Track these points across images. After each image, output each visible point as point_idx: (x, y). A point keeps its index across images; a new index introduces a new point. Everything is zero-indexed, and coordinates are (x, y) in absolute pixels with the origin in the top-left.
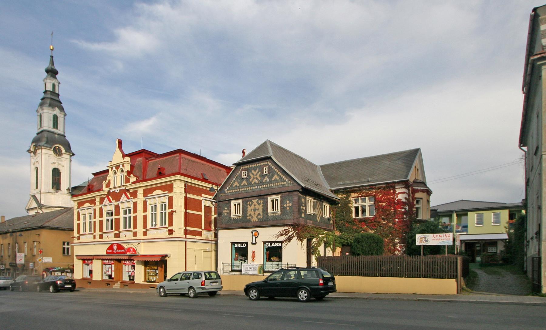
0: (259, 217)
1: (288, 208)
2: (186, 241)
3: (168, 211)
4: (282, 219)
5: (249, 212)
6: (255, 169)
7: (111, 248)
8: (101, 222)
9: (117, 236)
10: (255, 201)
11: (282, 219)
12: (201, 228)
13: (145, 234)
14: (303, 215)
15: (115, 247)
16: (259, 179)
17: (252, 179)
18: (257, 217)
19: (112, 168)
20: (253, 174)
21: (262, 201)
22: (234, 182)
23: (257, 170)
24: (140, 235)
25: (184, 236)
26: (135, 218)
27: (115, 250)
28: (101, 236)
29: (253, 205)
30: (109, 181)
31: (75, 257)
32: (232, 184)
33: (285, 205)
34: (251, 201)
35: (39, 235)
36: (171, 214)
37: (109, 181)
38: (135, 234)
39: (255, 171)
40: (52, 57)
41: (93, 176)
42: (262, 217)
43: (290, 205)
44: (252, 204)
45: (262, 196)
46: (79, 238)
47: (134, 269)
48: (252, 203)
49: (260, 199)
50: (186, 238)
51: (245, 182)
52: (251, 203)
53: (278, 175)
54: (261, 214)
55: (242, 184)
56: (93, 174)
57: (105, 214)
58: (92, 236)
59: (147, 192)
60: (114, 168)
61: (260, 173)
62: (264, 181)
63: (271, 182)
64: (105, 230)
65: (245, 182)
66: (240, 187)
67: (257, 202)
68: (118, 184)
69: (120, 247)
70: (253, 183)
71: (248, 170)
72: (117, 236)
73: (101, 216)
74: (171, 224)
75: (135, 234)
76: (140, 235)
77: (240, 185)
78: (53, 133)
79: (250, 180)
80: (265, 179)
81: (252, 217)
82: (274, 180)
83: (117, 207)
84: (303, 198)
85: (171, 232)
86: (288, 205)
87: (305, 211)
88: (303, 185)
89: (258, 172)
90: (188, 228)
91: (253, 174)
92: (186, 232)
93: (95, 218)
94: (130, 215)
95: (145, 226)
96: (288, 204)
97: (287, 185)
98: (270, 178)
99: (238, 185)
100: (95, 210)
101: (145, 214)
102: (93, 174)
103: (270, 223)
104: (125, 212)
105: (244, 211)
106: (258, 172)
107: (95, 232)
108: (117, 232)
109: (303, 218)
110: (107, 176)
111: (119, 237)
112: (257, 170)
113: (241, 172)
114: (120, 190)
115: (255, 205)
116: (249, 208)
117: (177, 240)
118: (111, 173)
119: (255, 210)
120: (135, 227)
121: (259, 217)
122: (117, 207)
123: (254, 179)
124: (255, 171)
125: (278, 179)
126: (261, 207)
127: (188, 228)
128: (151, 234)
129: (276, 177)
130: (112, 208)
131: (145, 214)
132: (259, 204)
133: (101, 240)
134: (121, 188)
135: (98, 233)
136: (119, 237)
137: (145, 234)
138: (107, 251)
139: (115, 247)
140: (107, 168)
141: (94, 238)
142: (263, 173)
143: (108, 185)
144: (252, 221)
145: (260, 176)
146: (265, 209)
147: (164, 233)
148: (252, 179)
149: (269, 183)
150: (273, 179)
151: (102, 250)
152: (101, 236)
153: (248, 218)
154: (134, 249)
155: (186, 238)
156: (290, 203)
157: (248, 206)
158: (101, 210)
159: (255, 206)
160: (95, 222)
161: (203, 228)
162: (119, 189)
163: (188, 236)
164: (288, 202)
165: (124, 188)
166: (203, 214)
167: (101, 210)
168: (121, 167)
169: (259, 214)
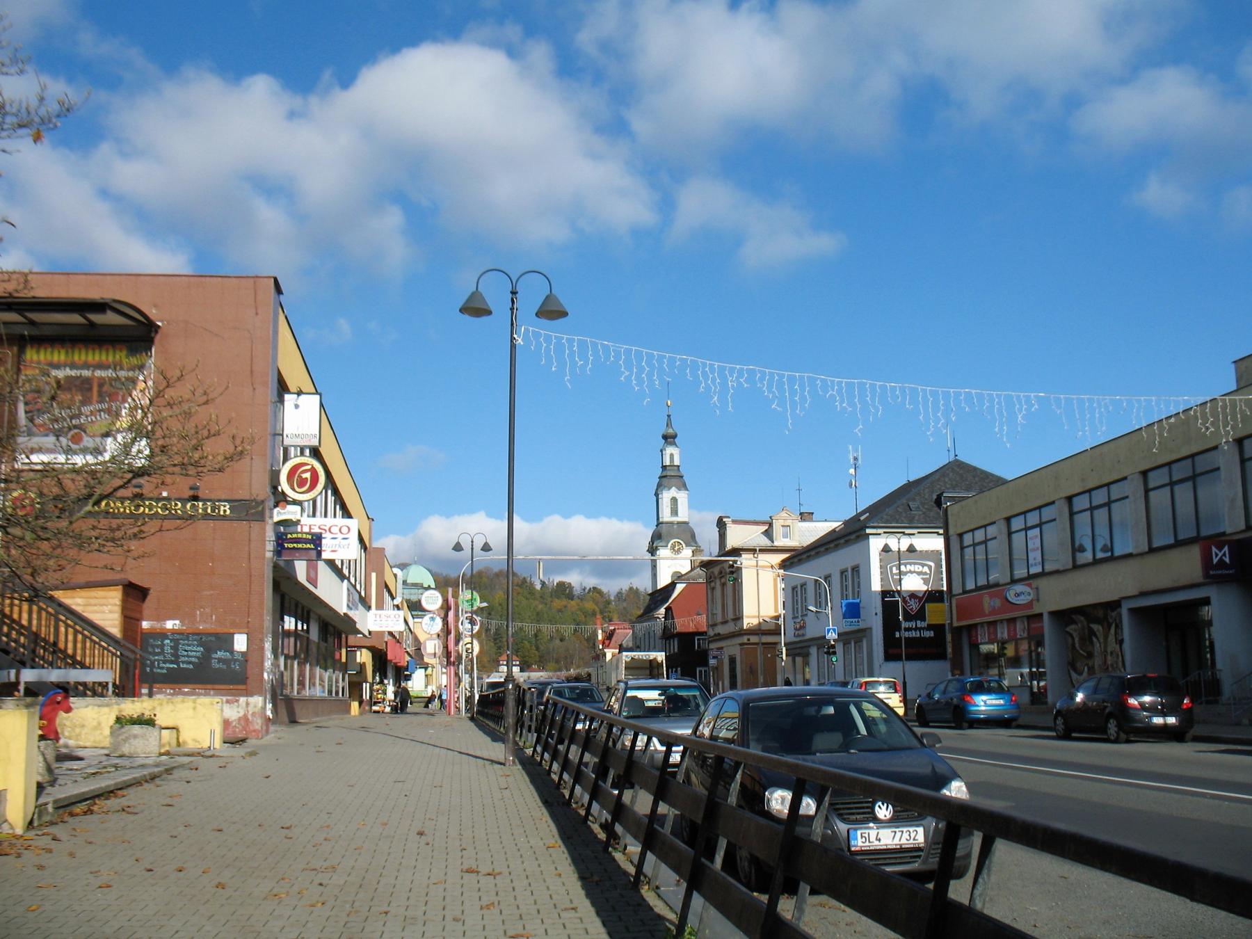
78: (672, 523)
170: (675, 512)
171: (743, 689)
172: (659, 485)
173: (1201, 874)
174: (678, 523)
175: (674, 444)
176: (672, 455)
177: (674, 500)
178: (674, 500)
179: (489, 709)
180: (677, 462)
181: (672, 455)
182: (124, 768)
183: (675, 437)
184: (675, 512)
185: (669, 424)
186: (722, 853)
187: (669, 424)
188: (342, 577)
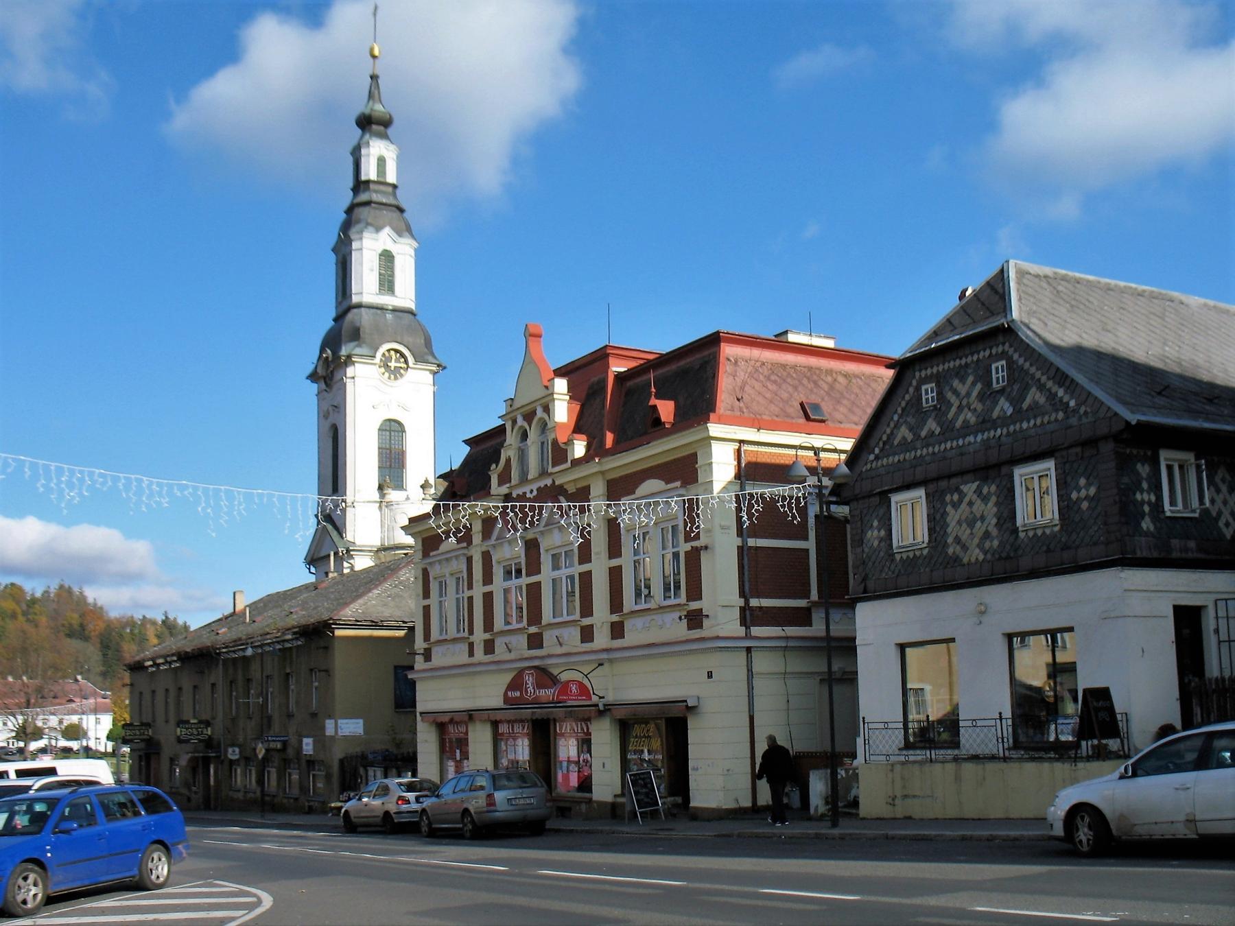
0: (987, 545)
1: (1085, 505)
2: (749, 650)
3: (684, 547)
4: (1066, 547)
5: (952, 528)
6: (960, 374)
7: (516, 683)
8: (488, 598)
9: (535, 641)
10: (969, 489)
11: (1066, 547)
12: (806, 594)
13: (617, 630)
14: (1147, 524)
15: (529, 680)
16: (979, 407)
17: (954, 409)
18: (980, 546)
19: (514, 422)
20: (955, 392)
21: (993, 488)
22: (897, 426)
23: (971, 379)
24: (602, 639)
25: (741, 631)
26: (586, 578)
27: (531, 689)
28: (489, 647)
29: (964, 506)
30: (508, 461)
31: (419, 718)
32: (891, 436)
33: (1074, 495)
34: (957, 489)
35: (326, 648)
36: (694, 559)
37: (508, 461)
38: (587, 634)
39: (963, 380)
40: (374, 77)
41: (467, 449)
42: (996, 543)
43: (1092, 491)
44: (960, 501)
45: (994, 470)
46: (427, 655)
47: (589, 751)
48: (962, 495)
49: (985, 480)
50: (748, 636)
51: (932, 425)
52: (956, 497)
53: (1041, 387)
54: (994, 532)
55: (923, 434)
56: (467, 442)
57: (498, 573)
58: (465, 647)
59: (619, 488)
60: (520, 421)
61: (979, 386)
62: (995, 414)
63: (1019, 415)
64: (499, 624)
65: (932, 425)
66: (918, 444)
67: (978, 492)
68: (533, 473)
69: (545, 676)
70: (959, 424)
71: (940, 380)
72: (535, 641)
73: (488, 579)
74: (695, 592)
75: (587, 634)
76: (602, 639)
77: (917, 437)
78: (381, 308)
79: (950, 416)
80: (998, 409)
81: (965, 548)
82: (1030, 408)
83: (532, 547)
84: (1144, 460)
85: (695, 619)
86: (1083, 493)
87: (1157, 506)
88: (1133, 418)
89: (974, 384)
90: (754, 602)
91: (955, 392)
92: (749, 617)
93: (470, 587)
94: (569, 571)
95: (616, 603)
96: (1084, 490)
97: (1032, 432)
98: (1016, 402)
99: (910, 437)
100: (469, 560)
101: (615, 562)
102: (467, 442)
103: (1025, 563)
104: (508, 574)
105: (936, 522)
106: (974, 384)
107: (471, 632)
108: (533, 630)
109: (1147, 534)
110: (501, 445)
111: (541, 646)
112: (971, 379)
113: (918, 389)
114: (539, 489)
115: (971, 504)
116: (953, 516)
117: (721, 645)
118: (511, 438)
119: (971, 523)
120: (587, 610)
121: (987, 545)
122: (532, 547)
123: (960, 408)
124: (963, 380)
125: (1042, 400)
126: (990, 509)
127: (754, 602)
128: (636, 632)
129: (1034, 396)
130: (516, 551)
131: (615, 562)
132: (985, 499)
133: (489, 658)
134: (542, 484)
135: (479, 636)
136: (541, 646)
137: (617, 630)
138: (505, 694)
139: (529, 680)
140: (500, 422)
141: (471, 654)
142: (989, 384)
143: (504, 478)
144: (965, 560)
145: (981, 397)
146: (1007, 515)
147: (675, 628)
148: (954, 409)
149: (1012, 419)
150: (1025, 406)
151: (489, 692)
152: (489, 647)
153: (950, 551)
154: (581, 685)
155: (748, 636)
156: (1088, 485)
157: (949, 508)
158: (487, 557)
159: (973, 505)
160: (470, 599)
161: (814, 595)
162: (535, 487)
163: (756, 631)
164: (1082, 481)
165: (549, 482)
166: (810, 544)
167: (487, 557)
168: (540, 413)
169: (987, 535)
170: (387, 283)
171: (528, 575)
172: (346, 226)
173: (324, 415)
174: (395, 310)
175: (384, 136)
176: (381, 161)
177: (387, 258)
178: (387, 258)
179: (317, 634)
180: (391, 177)
181: (381, 161)
182: (167, 697)
183: (386, 123)
184: (387, 283)
185: (373, 93)
186: (1144, 917)
187: (373, 93)
188: (315, 559)
